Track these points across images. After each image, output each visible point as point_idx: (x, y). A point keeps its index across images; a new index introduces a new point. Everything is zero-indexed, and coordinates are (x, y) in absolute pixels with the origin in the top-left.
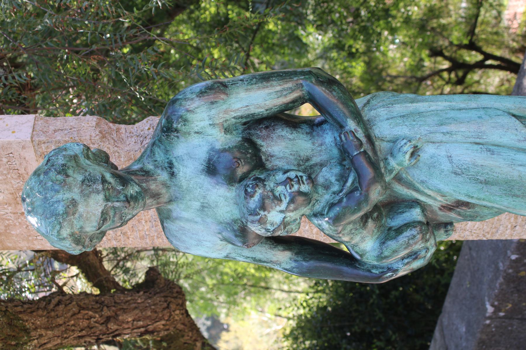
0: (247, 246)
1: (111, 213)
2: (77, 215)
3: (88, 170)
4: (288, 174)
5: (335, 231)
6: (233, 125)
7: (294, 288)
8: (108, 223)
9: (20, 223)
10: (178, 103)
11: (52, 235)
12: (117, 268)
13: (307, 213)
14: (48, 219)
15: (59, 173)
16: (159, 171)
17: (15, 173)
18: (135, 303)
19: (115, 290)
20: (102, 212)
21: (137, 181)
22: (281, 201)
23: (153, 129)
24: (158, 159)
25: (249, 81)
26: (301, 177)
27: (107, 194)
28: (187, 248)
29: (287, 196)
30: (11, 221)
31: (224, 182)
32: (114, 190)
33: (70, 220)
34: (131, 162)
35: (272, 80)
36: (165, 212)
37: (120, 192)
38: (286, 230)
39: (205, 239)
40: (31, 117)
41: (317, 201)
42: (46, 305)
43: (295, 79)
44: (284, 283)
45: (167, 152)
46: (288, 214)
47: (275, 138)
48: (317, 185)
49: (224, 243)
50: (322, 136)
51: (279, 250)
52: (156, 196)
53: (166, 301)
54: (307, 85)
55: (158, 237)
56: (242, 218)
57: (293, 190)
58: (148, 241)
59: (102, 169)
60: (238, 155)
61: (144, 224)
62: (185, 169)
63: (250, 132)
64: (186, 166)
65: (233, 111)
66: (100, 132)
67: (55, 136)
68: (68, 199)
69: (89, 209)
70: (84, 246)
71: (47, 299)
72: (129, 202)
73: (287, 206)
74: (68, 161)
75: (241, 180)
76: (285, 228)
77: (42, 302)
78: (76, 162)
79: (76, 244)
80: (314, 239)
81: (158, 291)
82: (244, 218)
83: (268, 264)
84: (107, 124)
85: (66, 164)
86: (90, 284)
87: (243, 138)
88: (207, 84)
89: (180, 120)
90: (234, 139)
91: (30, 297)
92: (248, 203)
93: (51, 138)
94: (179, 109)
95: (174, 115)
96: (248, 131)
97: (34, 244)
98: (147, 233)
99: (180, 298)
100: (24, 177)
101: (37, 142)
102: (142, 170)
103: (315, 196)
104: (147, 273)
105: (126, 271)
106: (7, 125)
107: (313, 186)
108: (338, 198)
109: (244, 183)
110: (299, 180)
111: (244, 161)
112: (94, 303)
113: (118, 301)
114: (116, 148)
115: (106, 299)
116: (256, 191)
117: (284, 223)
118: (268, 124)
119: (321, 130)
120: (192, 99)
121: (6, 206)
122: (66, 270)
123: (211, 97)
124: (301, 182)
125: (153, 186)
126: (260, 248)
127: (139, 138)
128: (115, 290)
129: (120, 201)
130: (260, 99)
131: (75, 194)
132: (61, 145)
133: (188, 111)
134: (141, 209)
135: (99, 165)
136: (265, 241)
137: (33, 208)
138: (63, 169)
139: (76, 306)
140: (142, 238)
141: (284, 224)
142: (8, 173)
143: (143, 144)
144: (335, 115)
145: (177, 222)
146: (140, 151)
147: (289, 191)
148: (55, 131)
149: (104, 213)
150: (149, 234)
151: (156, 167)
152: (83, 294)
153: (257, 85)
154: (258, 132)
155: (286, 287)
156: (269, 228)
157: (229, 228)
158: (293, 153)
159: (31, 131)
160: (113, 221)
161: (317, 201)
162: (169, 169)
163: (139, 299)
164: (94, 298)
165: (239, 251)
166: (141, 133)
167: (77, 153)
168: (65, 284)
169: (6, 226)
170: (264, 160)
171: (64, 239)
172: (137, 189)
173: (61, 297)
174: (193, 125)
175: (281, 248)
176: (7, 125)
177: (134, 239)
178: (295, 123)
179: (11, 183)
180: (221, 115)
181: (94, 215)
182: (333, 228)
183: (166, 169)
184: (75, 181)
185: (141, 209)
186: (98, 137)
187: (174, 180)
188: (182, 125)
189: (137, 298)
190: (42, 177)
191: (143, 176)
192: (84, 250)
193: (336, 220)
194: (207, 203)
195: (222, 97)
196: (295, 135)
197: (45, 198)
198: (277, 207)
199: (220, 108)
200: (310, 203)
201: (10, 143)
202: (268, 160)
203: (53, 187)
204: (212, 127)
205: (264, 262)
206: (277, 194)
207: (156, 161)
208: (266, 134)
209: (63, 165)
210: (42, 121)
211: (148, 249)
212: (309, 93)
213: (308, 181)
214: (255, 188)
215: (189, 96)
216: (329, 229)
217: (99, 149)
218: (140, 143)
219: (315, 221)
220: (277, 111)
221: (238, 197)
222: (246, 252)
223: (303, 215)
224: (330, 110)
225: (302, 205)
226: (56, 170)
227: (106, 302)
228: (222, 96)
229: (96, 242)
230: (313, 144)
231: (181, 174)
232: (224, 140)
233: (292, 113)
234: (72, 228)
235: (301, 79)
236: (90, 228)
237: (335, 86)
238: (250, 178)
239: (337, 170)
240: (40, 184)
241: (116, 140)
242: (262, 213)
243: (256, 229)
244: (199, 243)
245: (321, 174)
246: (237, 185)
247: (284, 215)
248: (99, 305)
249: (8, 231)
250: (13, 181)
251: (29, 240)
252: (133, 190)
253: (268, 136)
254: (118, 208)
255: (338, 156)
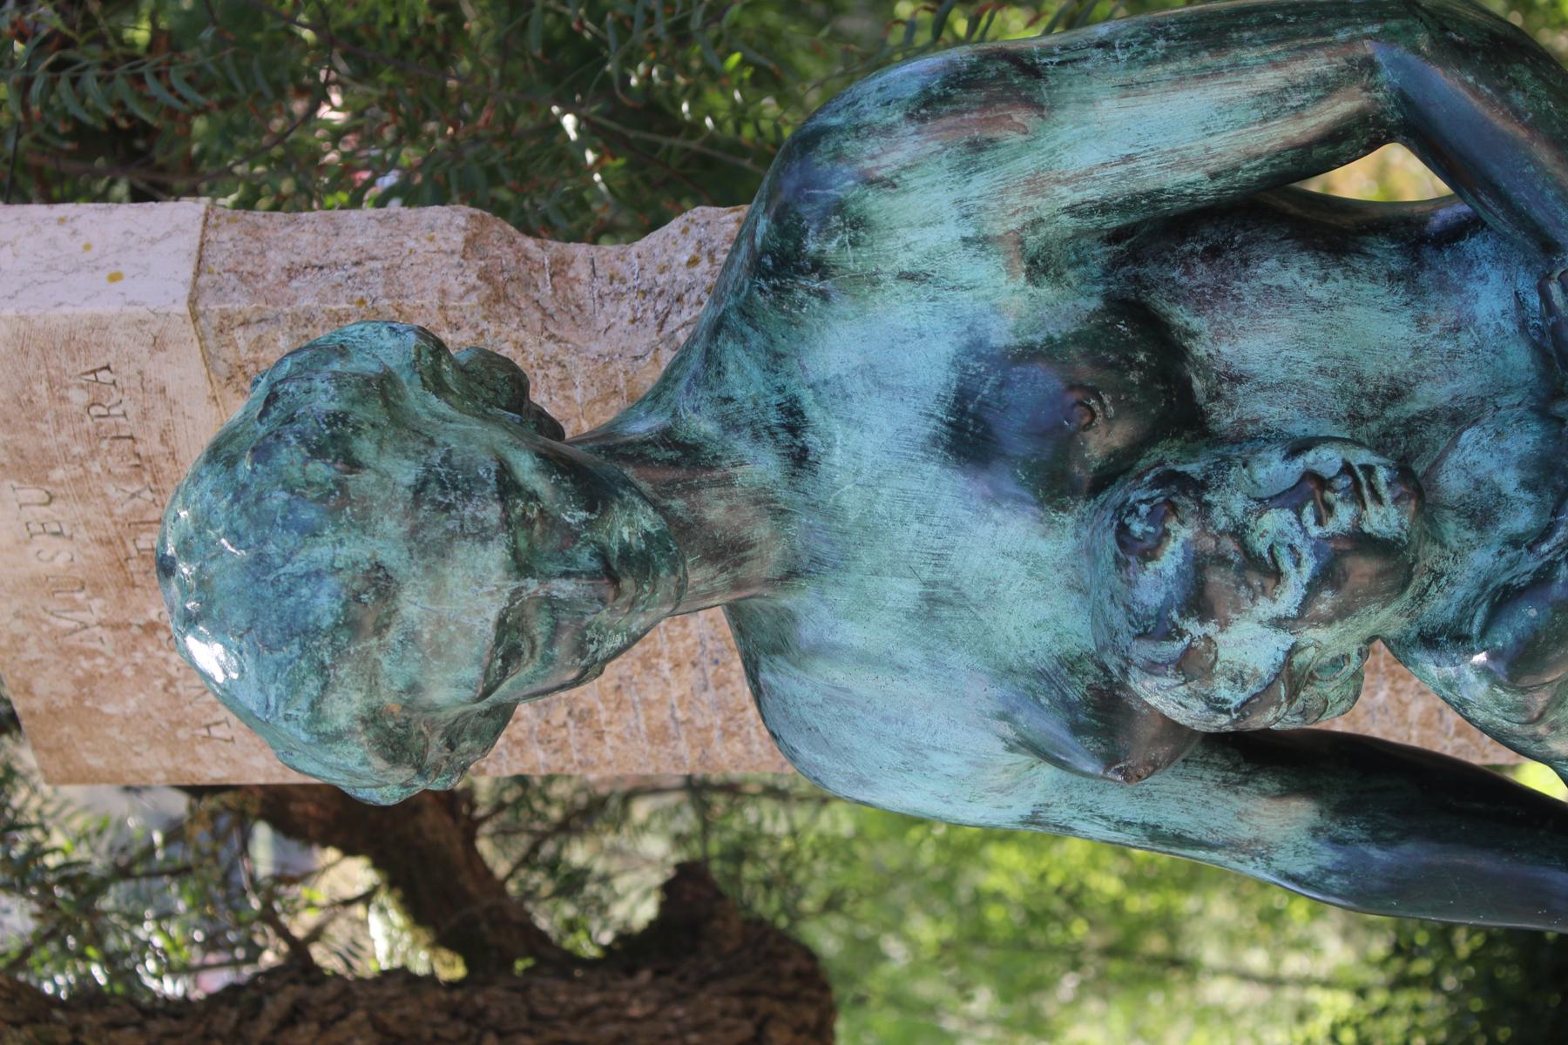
0: (1124, 772)
1: (539, 627)
2: (393, 636)
3: (439, 440)
4: (1310, 457)
5: (1516, 709)
6: (1066, 241)
7: (1294, 964)
8: (527, 669)
9: (139, 670)
10: (826, 146)
11: (287, 718)
12: (534, 868)
13: (1392, 632)
14: (270, 649)
15: (318, 452)
16: (742, 446)
17: (122, 455)
18: (616, 1019)
19: (529, 962)
20: (501, 623)
21: (645, 487)
22: (1277, 575)
23: (712, 259)
24: (739, 393)
25: (1136, 48)
26: (1369, 470)
27: (523, 544)
28: (861, 782)
29: (1305, 552)
30: (100, 661)
31: (1026, 494)
32: (552, 525)
33: (365, 656)
34: (617, 405)
35: (1241, 44)
36: (765, 621)
37: (575, 536)
38: (1299, 703)
39: (940, 740)
40: (185, 213)
41: (1438, 576)
42: (239, 1022)
43: (1341, 36)
44: (1253, 941)
45: (775, 360)
46: (1310, 635)
47: (1249, 299)
48: (1438, 505)
49: (1023, 759)
50: (1459, 290)
51: (1264, 793)
52: (728, 552)
53: (748, 1013)
54: (1396, 64)
55: (727, 734)
56: (1103, 648)
57: (1331, 526)
58: (683, 747)
59: (499, 436)
60: (1086, 372)
61: (667, 674)
62: (855, 434)
63: (1142, 271)
64: (859, 423)
65: (1068, 181)
66: (485, 276)
67: (289, 292)
68: (355, 564)
69: (447, 608)
70: (421, 771)
71: (243, 997)
72: (615, 580)
73: (1305, 598)
74: (353, 401)
75: (1102, 481)
76: (1293, 695)
77: (223, 1009)
78: (387, 404)
79: (388, 759)
80: (1414, 742)
81: (716, 967)
82: (1115, 649)
83: (1214, 855)
84: (511, 243)
85: (346, 414)
86: (425, 936)
87: (1107, 297)
88: (952, 63)
89: (835, 221)
90: (1066, 306)
91: (171, 988)
92: (1130, 584)
93: (276, 304)
94: (832, 173)
95: (811, 199)
96: (1130, 269)
97: (197, 760)
98: (679, 714)
99: (811, 1002)
100: (161, 470)
101: (216, 322)
102: (666, 438)
103: (1430, 555)
104: (669, 889)
105: (572, 883)
106: (87, 247)
107: (1419, 511)
108: (1531, 564)
109: (1116, 495)
110: (1356, 482)
111: (1112, 402)
112: (440, 1018)
113: (544, 1010)
114: (551, 347)
115: (495, 1000)
116: (1166, 533)
117: (1291, 675)
118: (1218, 237)
119: (1457, 260)
120: (888, 130)
121: (80, 596)
122: (305, 877)
123: (971, 124)
124: (1366, 492)
125: (716, 512)
126: (1179, 785)
127: (649, 304)
128: (529, 962)
129: (577, 575)
130: (1177, 127)
131: (386, 542)
132: (320, 334)
133: (870, 181)
134: (667, 609)
135: (485, 418)
136: (1200, 751)
137: (208, 604)
138: (333, 436)
139: (367, 1029)
140: (660, 735)
141: (1292, 676)
142: (93, 454)
143: (668, 329)
144: (1521, 196)
145: (820, 665)
146: (655, 360)
147: (1315, 531)
148: (291, 272)
149: (510, 627)
150: (689, 721)
151: (730, 425)
152: (401, 976)
153: (1172, 67)
154: (1175, 274)
155: (1257, 960)
156: (1224, 693)
157: (1047, 694)
158: (1330, 364)
159: (188, 272)
160: (548, 661)
161: (1438, 576)
162: (783, 435)
163: (636, 1002)
164: (443, 996)
165: (1089, 797)
166: (661, 279)
167: (392, 365)
168: (316, 934)
169: (79, 683)
170: (1201, 397)
171: (338, 736)
172: (647, 520)
173: (301, 990)
174: (889, 244)
175: (1271, 785)
176: (87, 247)
177: (624, 741)
178: (1340, 234)
179: (104, 495)
180: (1014, 199)
181: (467, 633)
182: (1507, 697)
183: (773, 435)
184: (384, 488)
185: (667, 609)
186: (473, 299)
187: (807, 483)
188: (842, 245)
189: (623, 997)
190: (246, 465)
191: (674, 464)
192: (421, 785)
193: (1521, 664)
194: (949, 585)
195: (1017, 119)
196: (1338, 284)
197: (260, 558)
198: (1262, 601)
199: (1012, 166)
200: (1404, 586)
201: (99, 325)
202: (1219, 396)
203: (292, 511)
204: (972, 250)
205: (1199, 844)
206: (1261, 546)
207: (729, 400)
208: (1209, 281)
209: (336, 418)
210: (234, 230)
211: (664, 784)
212: (1404, 99)
213: (1401, 489)
214: (1163, 520)
215: (875, 116)
216: (1490, 703)
217: (482, 351)
218: (653, 322)
219: (1433, 668)
220: (1262, 179)
221: (1085, 560)
222: (1119, 801)
223: (1371, 639)
224: (1497, 172)
225: (1371, 594)
226: (303, 440)
227: (494, 1013)
228: (1019, 116)
229: (470, 751)
230: (1421, 322)
231: (838, 457)
232: (1025, 311)
233: (1314, 186)
234: (373, 688)
235: (1368, 37)
236: (450, 689)
237: (1518, 67)
238: (1140, 476)
239: (1525, 441)
240: (236, 499)
241: (551, 309)
242: (1193, 627)
243: (1162, 697)
244: (914, 758)
245: (1454, 458)
246: (1083, 507)
247: (1292, 639)
248: (462, 1027)
249: (88, 703)
250: (111, 490)
251: (177, 741)
252: (630, 525)
253: (1219, 292)
254: (569, 603)
255: (1531, 376)
